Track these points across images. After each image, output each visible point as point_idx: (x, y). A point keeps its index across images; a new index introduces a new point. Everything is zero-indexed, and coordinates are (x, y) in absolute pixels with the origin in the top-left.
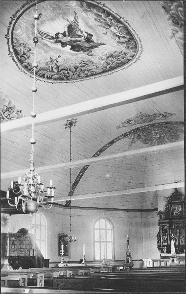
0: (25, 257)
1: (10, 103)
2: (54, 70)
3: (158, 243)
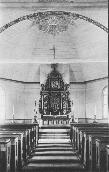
3: (39, 107)
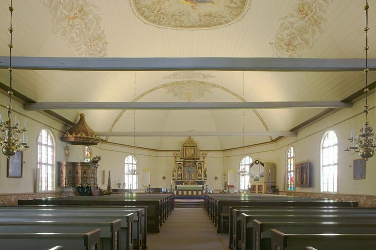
0: (268, 201)
1: (103, 32)
2: (155, 12)
